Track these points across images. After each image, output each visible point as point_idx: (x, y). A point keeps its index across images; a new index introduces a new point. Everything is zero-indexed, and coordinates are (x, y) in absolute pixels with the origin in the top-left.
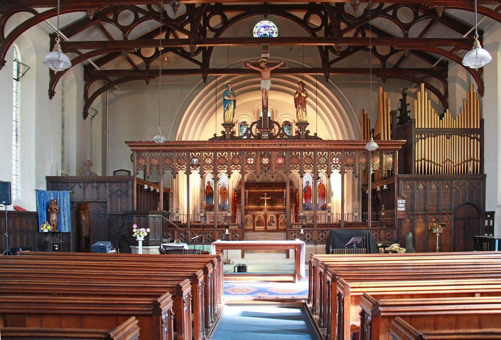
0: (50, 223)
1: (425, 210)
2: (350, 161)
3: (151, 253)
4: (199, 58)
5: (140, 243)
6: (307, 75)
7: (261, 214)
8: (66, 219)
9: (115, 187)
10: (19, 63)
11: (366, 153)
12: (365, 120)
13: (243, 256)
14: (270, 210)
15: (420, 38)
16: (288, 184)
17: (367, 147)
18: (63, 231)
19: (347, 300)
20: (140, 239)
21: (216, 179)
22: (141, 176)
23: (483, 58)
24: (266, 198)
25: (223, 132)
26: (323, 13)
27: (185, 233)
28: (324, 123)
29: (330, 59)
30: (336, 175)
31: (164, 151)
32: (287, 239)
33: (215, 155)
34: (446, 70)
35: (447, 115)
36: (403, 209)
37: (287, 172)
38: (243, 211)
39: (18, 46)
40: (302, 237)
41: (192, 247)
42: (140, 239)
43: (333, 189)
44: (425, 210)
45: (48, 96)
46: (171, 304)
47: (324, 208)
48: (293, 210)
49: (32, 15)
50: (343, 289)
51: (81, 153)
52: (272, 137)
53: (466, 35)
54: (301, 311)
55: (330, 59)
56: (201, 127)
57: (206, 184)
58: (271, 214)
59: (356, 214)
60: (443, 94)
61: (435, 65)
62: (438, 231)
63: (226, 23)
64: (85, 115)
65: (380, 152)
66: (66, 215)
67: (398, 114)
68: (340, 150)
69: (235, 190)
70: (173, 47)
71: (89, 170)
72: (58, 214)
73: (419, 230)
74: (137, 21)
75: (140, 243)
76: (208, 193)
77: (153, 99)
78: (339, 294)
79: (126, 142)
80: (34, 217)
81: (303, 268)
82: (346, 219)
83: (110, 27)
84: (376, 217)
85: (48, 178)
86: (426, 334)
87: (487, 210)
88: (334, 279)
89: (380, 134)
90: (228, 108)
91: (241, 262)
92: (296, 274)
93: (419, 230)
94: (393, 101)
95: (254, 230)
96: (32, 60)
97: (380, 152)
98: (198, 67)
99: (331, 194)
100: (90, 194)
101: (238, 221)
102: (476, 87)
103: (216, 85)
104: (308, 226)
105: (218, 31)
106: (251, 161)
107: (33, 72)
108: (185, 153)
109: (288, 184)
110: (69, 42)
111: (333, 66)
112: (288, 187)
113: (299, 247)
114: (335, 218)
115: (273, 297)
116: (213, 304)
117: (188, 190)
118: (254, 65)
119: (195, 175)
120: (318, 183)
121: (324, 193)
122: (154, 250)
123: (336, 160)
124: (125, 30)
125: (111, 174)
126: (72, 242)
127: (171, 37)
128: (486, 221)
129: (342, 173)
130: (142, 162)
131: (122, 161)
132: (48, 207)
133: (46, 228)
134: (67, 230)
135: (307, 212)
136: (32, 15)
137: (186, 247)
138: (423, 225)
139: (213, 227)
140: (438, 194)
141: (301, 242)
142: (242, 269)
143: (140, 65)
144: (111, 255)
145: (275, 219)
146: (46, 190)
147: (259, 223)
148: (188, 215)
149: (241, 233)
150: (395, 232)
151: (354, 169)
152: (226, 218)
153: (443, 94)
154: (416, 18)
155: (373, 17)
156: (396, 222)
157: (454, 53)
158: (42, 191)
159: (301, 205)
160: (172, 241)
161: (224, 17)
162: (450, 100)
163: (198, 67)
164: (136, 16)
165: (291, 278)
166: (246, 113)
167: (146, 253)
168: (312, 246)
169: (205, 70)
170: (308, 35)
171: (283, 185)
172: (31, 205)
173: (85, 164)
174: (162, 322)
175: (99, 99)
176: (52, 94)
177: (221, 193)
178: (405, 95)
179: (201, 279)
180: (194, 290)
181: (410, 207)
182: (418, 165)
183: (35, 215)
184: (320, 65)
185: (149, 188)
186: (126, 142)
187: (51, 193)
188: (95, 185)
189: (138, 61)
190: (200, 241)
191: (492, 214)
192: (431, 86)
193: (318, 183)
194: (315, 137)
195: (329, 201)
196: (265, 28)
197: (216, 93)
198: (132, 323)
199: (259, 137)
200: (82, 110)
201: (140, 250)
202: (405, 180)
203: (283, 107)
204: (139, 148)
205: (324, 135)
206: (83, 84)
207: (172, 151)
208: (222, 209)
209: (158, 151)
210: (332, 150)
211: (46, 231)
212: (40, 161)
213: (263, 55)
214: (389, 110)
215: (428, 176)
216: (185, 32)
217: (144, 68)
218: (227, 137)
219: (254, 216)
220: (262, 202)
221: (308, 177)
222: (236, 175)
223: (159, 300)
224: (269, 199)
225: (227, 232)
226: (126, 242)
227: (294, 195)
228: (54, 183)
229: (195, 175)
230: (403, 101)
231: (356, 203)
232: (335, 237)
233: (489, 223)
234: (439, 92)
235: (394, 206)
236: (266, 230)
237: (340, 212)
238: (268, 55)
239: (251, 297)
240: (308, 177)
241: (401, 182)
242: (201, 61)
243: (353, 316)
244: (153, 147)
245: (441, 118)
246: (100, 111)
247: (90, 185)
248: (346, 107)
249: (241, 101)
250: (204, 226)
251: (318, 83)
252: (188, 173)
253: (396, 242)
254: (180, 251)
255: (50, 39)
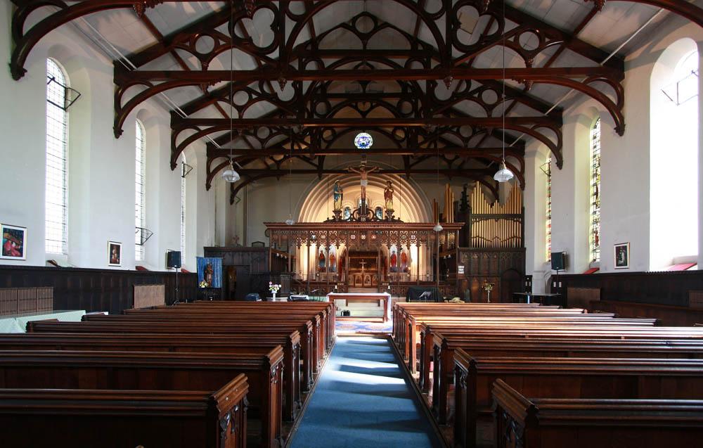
0: (206, 281)
1: (479, 273)
2: (424, 237)
3: (281, 301)
4: (316, 162)
5: (274, 295)
6: (395, 175)
7: (360, 274)
8: (219, 278)
9: (256, 255)
10: (184, 164)
11: (436, 234)
12: (435, 206)
13: (347, 305)
14: (366, 272)
15: (477, 148)
16: (379, 253)
17: (435, 229)
18: (216, 287)
19: (414, 328)
20: (274, 292)
21: (328, 249)
22: (273, 247)
23: (507, 176)
24: (363, 263)
25: (333, 217)
26: (425, 59)
27: (306, 289)
28: (405, 209)
29: (411, 163)
30: (413, 247)
31: (291, 229)
32: (379, 292)
33: (328, 232)
34: (523, 149)
35: (496, 203)
36: (463, 273)
37: (379, 245)
38: (347, 273)
39: (64, 66)
40: (388, 291)
41: (312, 298)
42: (274, 292)
43: (412, 257)
44: (479, 273)
45: (113, 135)
46: (281, 358)
47: (406, 270)
48: (383, 272)
49: (197, 132)
50: (411, 321)
51: (229, 230)
52: (368, 220)
53: (511, 145)
54: (405, 381)
55: (411, 163)
56: (319, 211)
57: (320, 252)
58: (367, 275)
59: (428, 276)
60: (556, 145)
61: (489, 166)
62: (489, 289)
63: (335, 136)
64: (232, 202)
65: (445, 232)
66: (219, 275)
67: (460, 203)
68: (416, 230)
69: (341, 257)
70: (298, 154)
71: (236, 242)
72: (213, 275)
73: (475, 288)
74: (251, 102)
75: (274, 295)
76: (321, 259)
77: (284, 190)
78: (410, 325)
79: (264, 223)
80: (194, 276)
81: (390, 313)
82: (421, 279)
83: (250, 138)
84: (443, 278)
85: (205, 248)
86: (477, 359)
87: (527, 274)
88: (407, 316)
89: (445, 219)
90: (337, 200)
91: (346, 309)
92: (385, 317)
93: (475, 288)
94: (454, 193)
95: (354, 286)
96: (194, 162)
97: (445, 232)
98: (315, 168)
99: (411, 260)
100: (237, 260)
101: (343, 279)
102: (519, 184)
103: (328, 180)
104: (393, 283)
105: (330, 142)
106: (353, 237)
107: (195, 171)
108: (308, 231)
109: (379, 253)
110: (220, 149)
111: (413, 168)
112: (379, 256)
113: (386, 298)
114: (413, 278)
115: (370, 331)
116: (331, 335)
117: (306, 257)
118: (356, 169)
119: (313, 246)
120: (401, 253)
121: (406, 260)
122: (284, 300)
123: (413, 237)
124: (262, 141)
125: (250, 246)
126: (223, 293)
127: (296, 147)
128: (560, 286)
129: (418, 246)
130: (276, 237)
131: (258, 235)
132: (205, 270)
133: (203, 285)
134: (219, 286)
135: (393, 274)
136: (197, 132)
137: (308, 298)
138: (477, 284)
139: (326, 283)
140: (489, 262)
141: (389, 295)
142: (347, 314)
143: (272, 165)
144: (259, 302)
145: (370, 278)
146: (203, 256)
147: (358, 281)
148: (308, 275)
149: (345, 288)
150: (457, 289)
151: (427, 243)
152: (335, 277)
153: (556, 145)
154: (474, 133)
155: (459, 100)
156: (457, 282)
157: (588, 84)
158: (201, 258)
159: (389, 268)
160: (298, 294)
161: (328, 105)
162: (500, 192)
163: (315, 168)
164: (217, 44)
165: (381, 320)
166: (350, 202)
167: (278, 301)
168: (397, 298)
169: (320, 171)
170: (395, 146)
171: (375, 253)
172: (193, 268)
173: (231, 238)
174: (293, 352)
175: (241, 190)
176: (208, 187)
177: (331, 259)
178: (465, 189)
179: (325, 316)
180: (322, 321)
181: (467, 271)
182: (473, 241)
183: (195, 276)
184: (402, 167)
185: (280, 256)
186: (264, 223)
187: (208, 259)
188: (241, 253)
189: (270, 162)
190: (317, 294)
191: (531, 277)
192: (543, 136)
193: (401, 253)
194: (399, 221)
195: (409, 265)
196: (363, 139)
197: (328, 185)
198: (242, 379)
199: (359, 221)
200: (229, 198)
201: (274, 299)
202: (464, 251)
203: (376, 196)
204: (272, 228)
205: (405, 219)
206: (205, 159)
207: (297, 230)
208: (331, 270)
209: (288, 229)
210: (411, 230)
211: (203, 287)
212: (200, 235)
213: (363, 162)
214: (453, 201)
215: (480, 250)
216: (306, 144)
217: (276, 168)
218: (337, 220)
219: (354, 276)
220: (361, 266)
221: (394, 248)
222: (342, 246)
223: (269, 356)
224: (366, 263)
225: (336, 288)
226: (266, 294)
227: (384, 260)
228: (209, 252)
229: (313, 246)
230: (464, 193)
231: (429, 268)
232: (412, 291)
233: (528, 284)
234: (551, 143)
235: (456, 270)
236: (363, 287)
237: (416, 274)
238: (366, 162)
239: (354, 331)
240: (394, 248)
241: (461, 253)
242: (317, 164)
243: (417, 338)
244: (283, 227)
245: (491, 207)
246: (242, 199)
247: (237, 253)
248: (422, 197)
249: (346, 192)
250: (320, 283)
251: (402, 179)
252: (309, 245)
253: (457, 296)
254: (304, 300)
255: (170, 117)
